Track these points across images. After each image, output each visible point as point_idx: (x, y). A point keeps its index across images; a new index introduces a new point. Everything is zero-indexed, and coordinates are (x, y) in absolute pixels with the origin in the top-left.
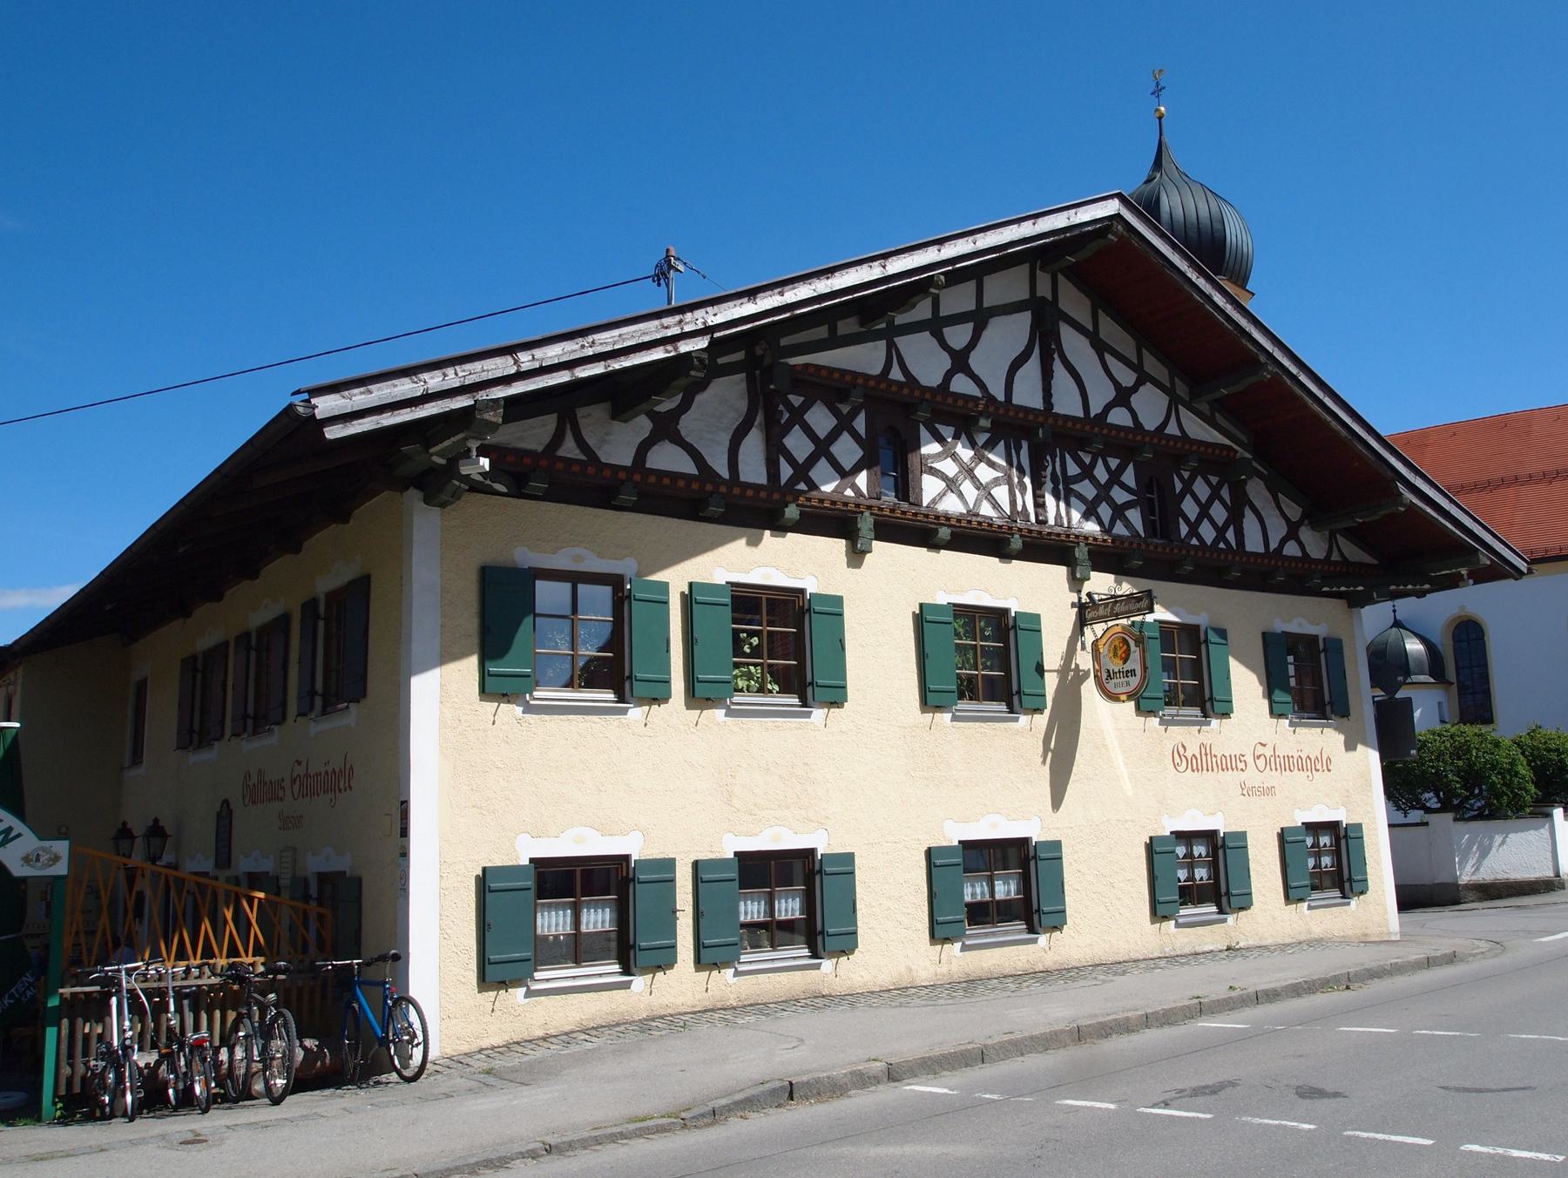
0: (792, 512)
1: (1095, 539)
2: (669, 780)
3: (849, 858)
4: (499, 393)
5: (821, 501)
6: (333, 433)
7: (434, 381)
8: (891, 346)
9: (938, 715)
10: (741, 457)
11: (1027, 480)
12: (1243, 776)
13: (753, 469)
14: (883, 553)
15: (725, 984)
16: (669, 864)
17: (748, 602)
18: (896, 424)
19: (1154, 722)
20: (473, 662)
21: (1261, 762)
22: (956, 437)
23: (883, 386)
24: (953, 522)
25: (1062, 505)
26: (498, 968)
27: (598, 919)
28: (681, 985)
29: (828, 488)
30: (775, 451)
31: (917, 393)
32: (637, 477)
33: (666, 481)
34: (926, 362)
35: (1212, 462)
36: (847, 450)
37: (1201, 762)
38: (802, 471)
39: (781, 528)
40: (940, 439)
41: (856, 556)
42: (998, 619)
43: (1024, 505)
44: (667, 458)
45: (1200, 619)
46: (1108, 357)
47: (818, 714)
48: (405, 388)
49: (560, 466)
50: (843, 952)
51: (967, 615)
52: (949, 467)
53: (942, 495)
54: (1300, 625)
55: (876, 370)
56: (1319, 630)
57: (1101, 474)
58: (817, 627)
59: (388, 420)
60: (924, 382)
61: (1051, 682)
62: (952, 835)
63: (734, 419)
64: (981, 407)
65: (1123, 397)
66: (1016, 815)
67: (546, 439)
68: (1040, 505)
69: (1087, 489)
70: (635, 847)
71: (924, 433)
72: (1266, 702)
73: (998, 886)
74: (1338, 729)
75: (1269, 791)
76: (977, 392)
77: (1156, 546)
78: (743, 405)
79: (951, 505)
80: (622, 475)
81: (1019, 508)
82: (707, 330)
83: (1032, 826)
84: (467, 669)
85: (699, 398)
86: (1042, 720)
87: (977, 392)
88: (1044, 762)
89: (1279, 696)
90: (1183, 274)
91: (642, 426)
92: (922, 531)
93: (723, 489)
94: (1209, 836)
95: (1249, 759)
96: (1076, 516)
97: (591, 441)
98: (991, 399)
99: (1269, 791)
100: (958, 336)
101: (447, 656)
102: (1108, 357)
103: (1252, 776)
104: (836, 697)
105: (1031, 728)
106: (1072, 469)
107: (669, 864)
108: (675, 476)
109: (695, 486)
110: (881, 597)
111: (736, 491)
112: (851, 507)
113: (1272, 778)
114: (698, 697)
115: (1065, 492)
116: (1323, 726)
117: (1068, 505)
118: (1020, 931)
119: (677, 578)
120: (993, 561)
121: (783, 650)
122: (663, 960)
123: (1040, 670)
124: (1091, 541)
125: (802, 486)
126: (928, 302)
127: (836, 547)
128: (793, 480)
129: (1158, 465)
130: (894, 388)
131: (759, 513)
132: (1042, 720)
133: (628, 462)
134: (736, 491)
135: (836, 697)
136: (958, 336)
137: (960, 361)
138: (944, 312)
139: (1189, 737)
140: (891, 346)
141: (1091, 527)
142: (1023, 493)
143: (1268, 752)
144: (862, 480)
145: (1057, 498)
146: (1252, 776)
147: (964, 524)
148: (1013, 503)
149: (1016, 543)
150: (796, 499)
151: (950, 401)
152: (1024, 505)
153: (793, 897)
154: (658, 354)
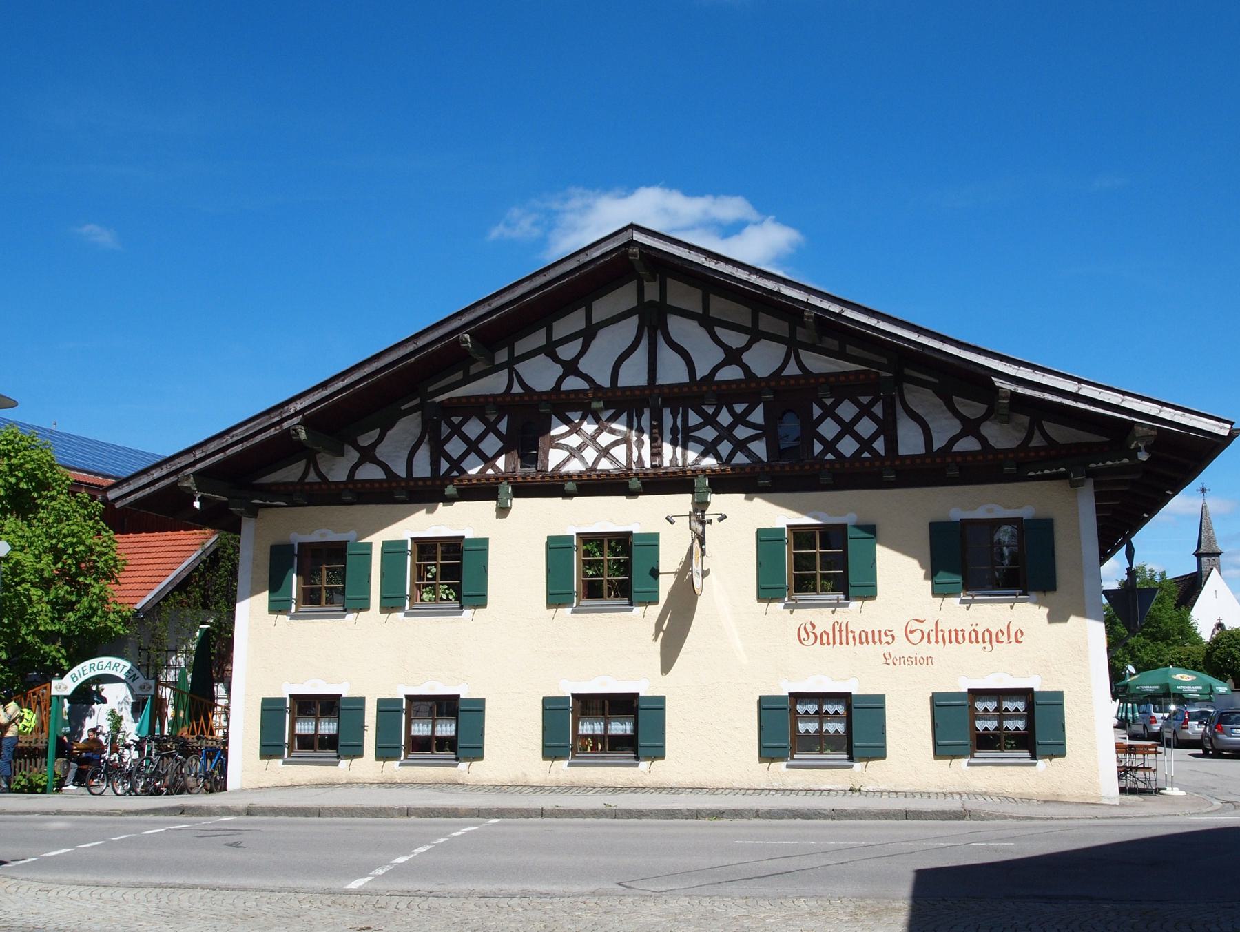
0: (450, 490)
1: (713, 471)
2: (371, 653)
3: (481, 702)
4: (189, 471)
5: (470, 480)
6: (118, 505)
7: (156, 474)
8: (512, 371)
9: (560, 610)
10: (414, 463)
11: (646, 438)
12: (887, 648)
13: (422, 468)
14: (519, 505)
15: (393, 769)
16: (361, 701)
17: (425, 547)
18: (527, 424)
19: (778, 607)
20: (267, 593)
21: (916, 637)
22: (583, 418)
23: (508, 399)
24: (575, 478)
25: (679, 450)
26: (270, 749)
27: (620, 728)
28: (367, 766)
29: (473, 472)
30: (438, 453)
31: (535, 398)
32: (350, 486)
33: (368, 485)
34: (541, 375)
35: (841, 387)
36: (491, 444)
37: (837, 636)
38: (456, 464)
39: (449, 500)
40: (567, 421)
41: (503, 511)
42: (623, 541)
43: (640, 456)
44: (370, 472)
45: (849, 518)
46: (719, 331)
47: (467, 613)
48: (145, 480)
49: (307, 487)
50: (355, 757)
51: (592, 540)
52: (574, 441)
53: (565, 462)
54: (989, 511)
55: (502, 390)
56: (1026, 512)
57: (725, 418)
58: (468, 560)
59: (140, 494)
60: (538, 389)
61: (666, 584)
62: (566, 689)
63: (411, 441)
64: (590, 396)
65: (733, 356)
66: (636, 675)
67: (300, 475)
68: (656, 453)
69: (709, 434)
70: (346, 691)
71: (554, 419)
72: (929, 583)
73: (612, 725)
74: (1040, 603)
75: (927, 660)
76: (585, 386)
77: (783, 467)
78: (418, 431)
79: (575, 466)
80: (342, 486)
81: (635, 458)
82: (296, 414)
83: (644, 689)
84: (263, 598)
85: (390, 433)
86: (655, 611)
87: (585, 386)
88: (656, 639)
89: (943, 577)
90: (701, 266)
91: (354, 455)
92: (555, 487)
93: (403, 484)
94: (1026, 694)
95: (899, 634)
96: (692, 456)
97: (323, 471)
98: (599, 388)
99: (927, 660)
100: (567, 352)
101: (254, 592)
102: (719, 331)
103: (901, 647)
104: (479, 601)
105: (643, 619)
106: (694, 419)
107: (361, 701)
108: (372, 482)
109: (385, 485)
110: (517, 537)
111: (412, 484)
112: (492, 480)
113: (924, 649)
114: (391, 604)
115: (683, 438)
116: (1014, 602)
117: (685, 447)
118: (628, 758)
119: (376, 541)
120: (622, 499)
121: (452, 574)
122: (356, 752)
123: (655, 573)
124: (709, 472)
125: (455, 473)
126: (543, 332)
127: (488, 507)
128: (449, 471)
129: (787, 399)
130: (517, 398)
131: (429, 493)
132: (655, 611)
133: (344, 478)
134: (412, 484)
135: (479, 601)
136: (567, 352)
137: (571, 368)
138: (556, 337)
139: (822, 618)
140: (512, 371)
141: (710, 462)
142: (640, 448)
143: (926, 627)
144: (501, 463)
145: (674, 443)
146: (901, 647)
147: (585, 478)
148: (629, 456)
149: (635, 484)
150: (451, 482)
151: (563, 396)
152: (640, 456)
153: (443, 726)
154: (272, 432)
